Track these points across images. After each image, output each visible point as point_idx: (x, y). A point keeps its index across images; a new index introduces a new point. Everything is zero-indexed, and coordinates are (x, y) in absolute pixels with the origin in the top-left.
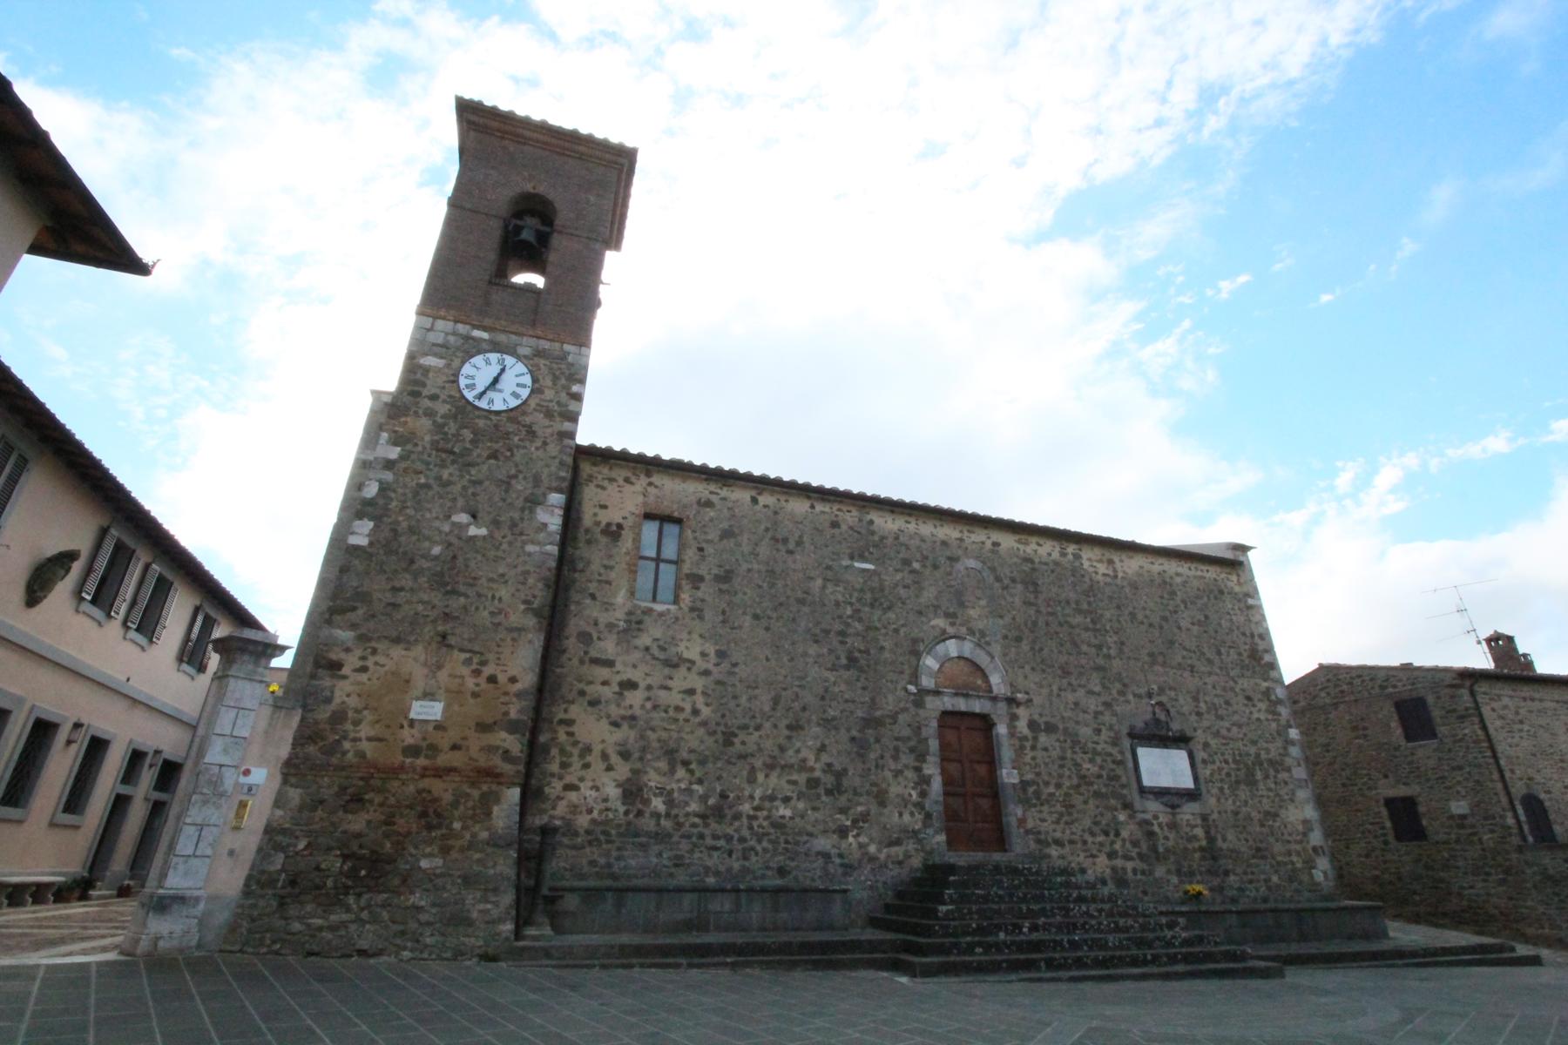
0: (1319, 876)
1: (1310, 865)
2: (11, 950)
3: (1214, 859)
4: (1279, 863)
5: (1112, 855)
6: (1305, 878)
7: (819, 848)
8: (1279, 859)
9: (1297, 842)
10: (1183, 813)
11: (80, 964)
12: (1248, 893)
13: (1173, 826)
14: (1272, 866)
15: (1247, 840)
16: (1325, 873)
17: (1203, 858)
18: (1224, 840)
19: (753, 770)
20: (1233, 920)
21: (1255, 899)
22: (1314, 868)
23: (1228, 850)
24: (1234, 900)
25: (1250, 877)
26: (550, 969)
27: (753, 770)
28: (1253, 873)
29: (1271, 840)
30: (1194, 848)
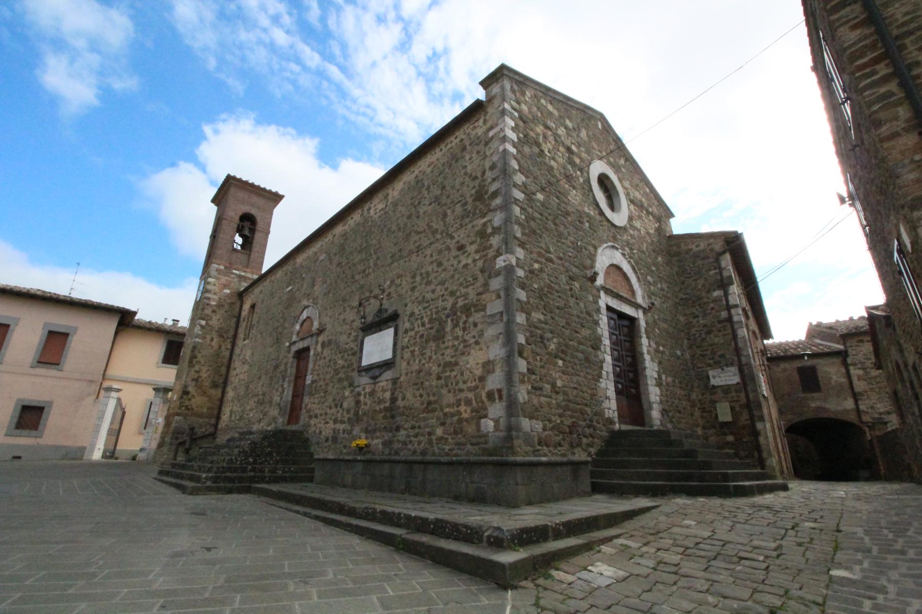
0: (488, 425)
1: (480, 413)
2: (882, 191)
3: (393, 417)
4: (445, 415)
5: (335, 421)
6: (470, 429)
7: (494, 327)
8: (447, 410)
9: (470, 390)
10: (381, 381)
11: (390, 534)
12: (410, 446)
13: (372, 393)
14: (438, 419)
15: (421, 396)
16: (497, 421)
17: (384, 417)
18: (403, 399)
19: (344, 308)
20: (359, 467)
21: (415, 452)
22: (485, 416)
23: (405, 407)
24: (397, 453)
25: (417, 430)
26: (685, 590)
27: (344, 308)
28: (419, 427)
29: (444, 391)
30: (380, 409)
